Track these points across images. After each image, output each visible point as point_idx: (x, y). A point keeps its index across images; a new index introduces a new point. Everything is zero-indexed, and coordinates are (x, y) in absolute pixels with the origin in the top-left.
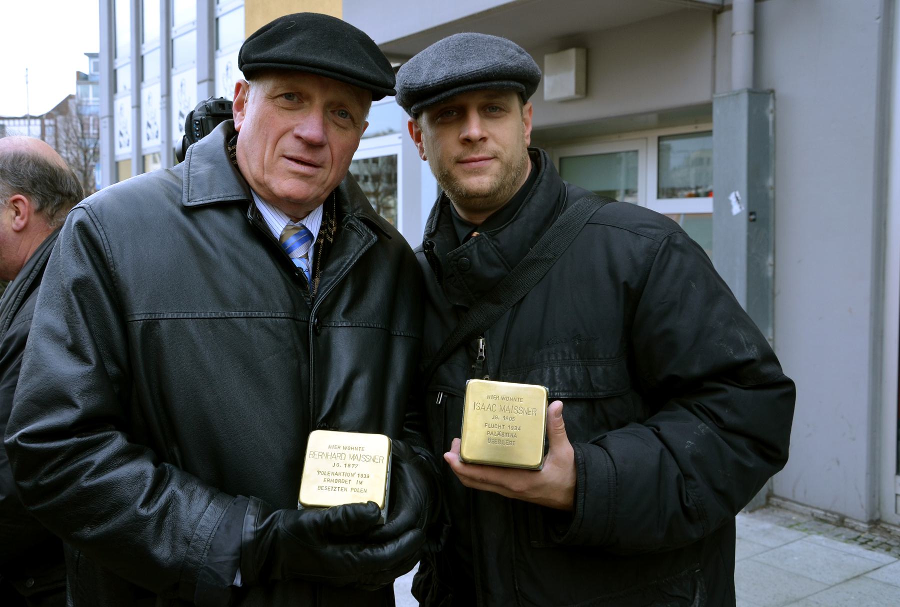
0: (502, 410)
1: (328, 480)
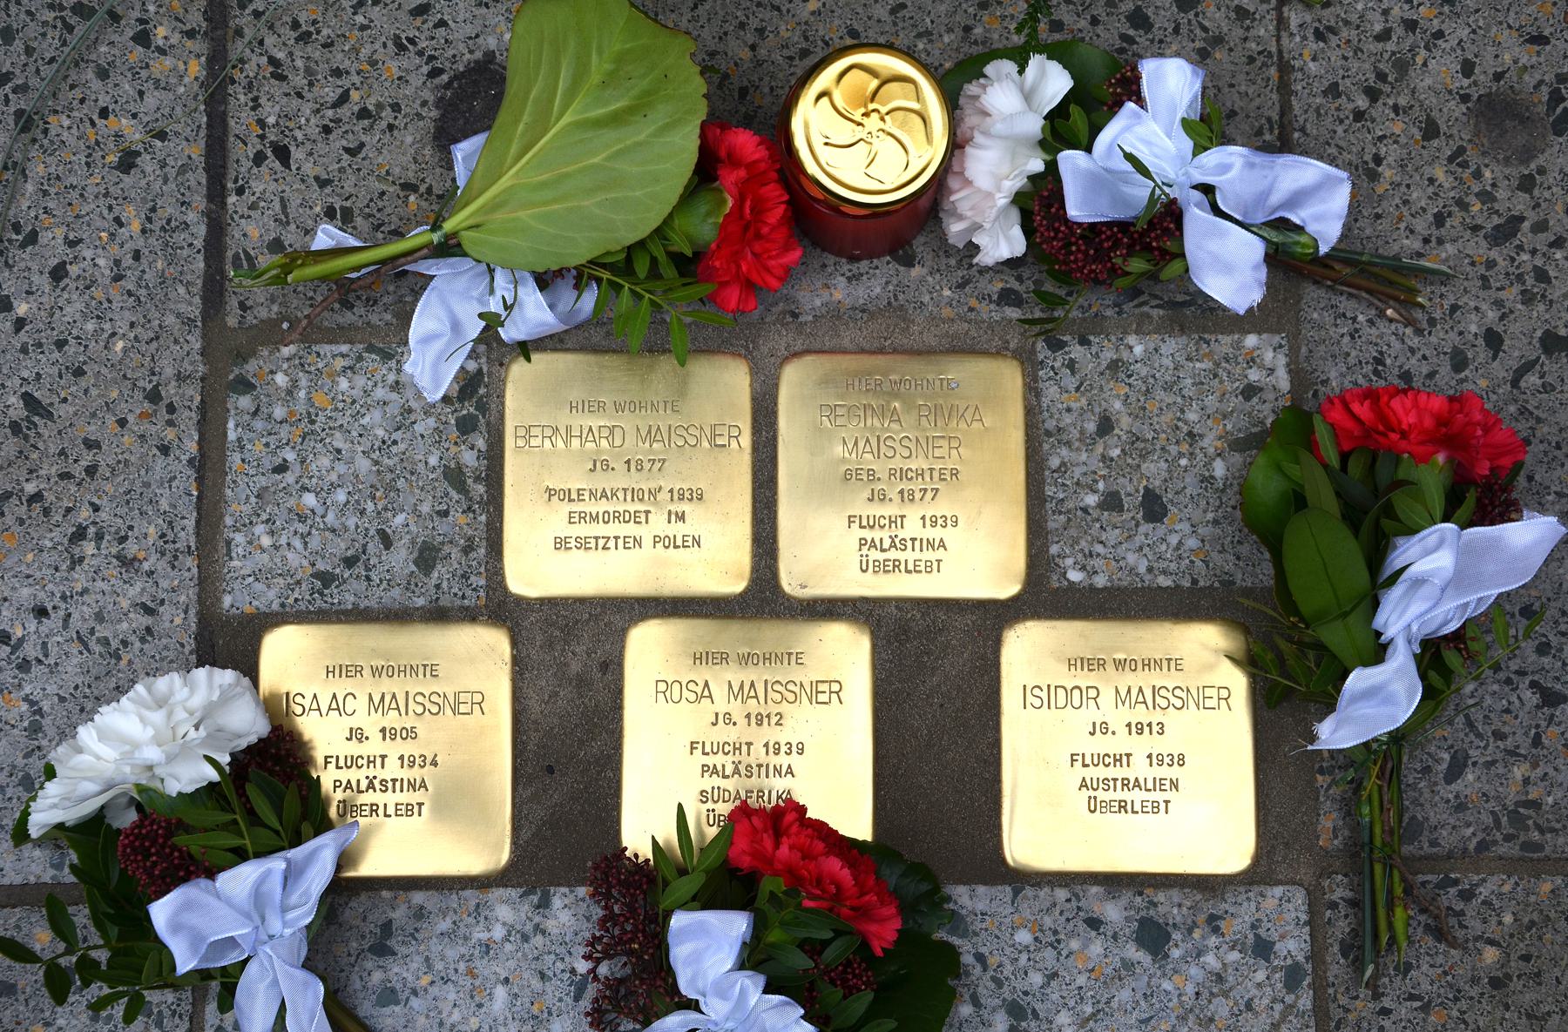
0: (1123, 703)
1: (583, 517)
